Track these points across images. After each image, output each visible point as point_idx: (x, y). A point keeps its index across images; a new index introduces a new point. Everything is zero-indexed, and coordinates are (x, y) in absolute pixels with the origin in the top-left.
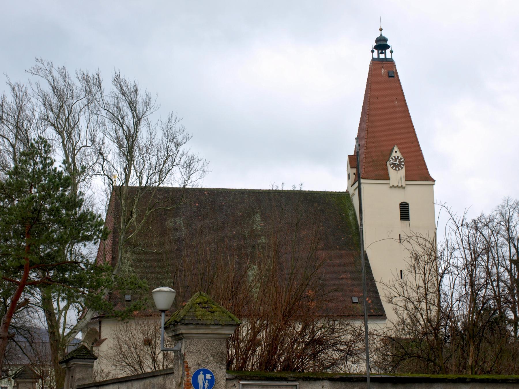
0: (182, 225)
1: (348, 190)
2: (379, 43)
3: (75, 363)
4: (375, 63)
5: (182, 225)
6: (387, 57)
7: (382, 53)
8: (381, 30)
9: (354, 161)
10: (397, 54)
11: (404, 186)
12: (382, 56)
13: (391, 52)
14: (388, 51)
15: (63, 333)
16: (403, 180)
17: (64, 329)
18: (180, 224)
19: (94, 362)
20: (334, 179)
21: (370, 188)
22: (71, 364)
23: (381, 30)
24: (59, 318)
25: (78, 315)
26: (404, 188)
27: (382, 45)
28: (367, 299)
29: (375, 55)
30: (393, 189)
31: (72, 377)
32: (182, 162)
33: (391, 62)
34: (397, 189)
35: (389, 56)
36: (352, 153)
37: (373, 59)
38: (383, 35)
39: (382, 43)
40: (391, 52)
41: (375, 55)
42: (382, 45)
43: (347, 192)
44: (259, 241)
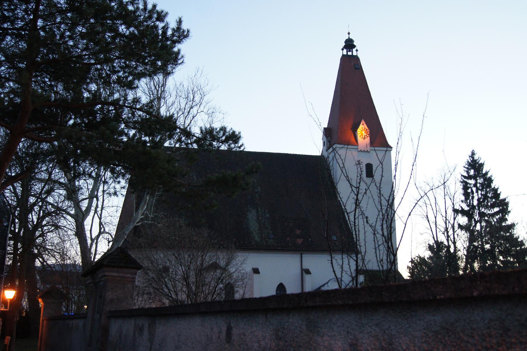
0: (194, 177)
1: (323, 154)
2: (348, 43)
3: (106, 274)
4: (345, 59)
5: (194, 177)
6: (354, 54)
7: (350, 51)
8: (349, 34)
9: (327, 132)
10: (361, 52)
11: (369, 150)
12: (350, 53)
13: (357, 50)
14: (354, 50)
15: (94, 258)
16: (368, 146)
17: (95, 254)
18: (193, 176)
19: (136, 274)
20: (312, 145)
21: (342, 151)
22: (100, 276)
23: (349, 34)
24: (91, 245)
25: (108, 245)
26: (369, 152)
27: (349, 45)
28: (343, 237)
29: (345, 53)
30: (361, 153)
31: (101, 297)
32: (205, 110)
33: (357, 58)
34: (364, 153)
35: (355, 53)
36: (326, 126)
37: (343, 55)
38: (350, 37)
39: (350, 43)
40: (357, 50)
41: (345, 53)
42: (349, 45)
43: (322, 156)
44: (256, 190)
